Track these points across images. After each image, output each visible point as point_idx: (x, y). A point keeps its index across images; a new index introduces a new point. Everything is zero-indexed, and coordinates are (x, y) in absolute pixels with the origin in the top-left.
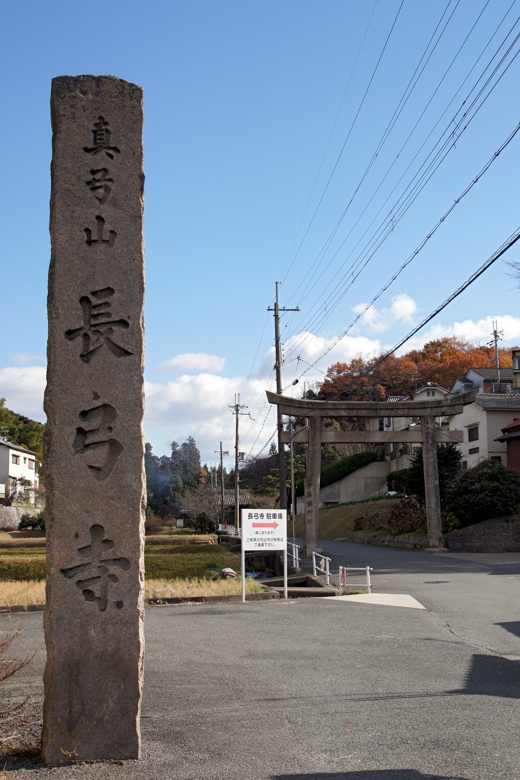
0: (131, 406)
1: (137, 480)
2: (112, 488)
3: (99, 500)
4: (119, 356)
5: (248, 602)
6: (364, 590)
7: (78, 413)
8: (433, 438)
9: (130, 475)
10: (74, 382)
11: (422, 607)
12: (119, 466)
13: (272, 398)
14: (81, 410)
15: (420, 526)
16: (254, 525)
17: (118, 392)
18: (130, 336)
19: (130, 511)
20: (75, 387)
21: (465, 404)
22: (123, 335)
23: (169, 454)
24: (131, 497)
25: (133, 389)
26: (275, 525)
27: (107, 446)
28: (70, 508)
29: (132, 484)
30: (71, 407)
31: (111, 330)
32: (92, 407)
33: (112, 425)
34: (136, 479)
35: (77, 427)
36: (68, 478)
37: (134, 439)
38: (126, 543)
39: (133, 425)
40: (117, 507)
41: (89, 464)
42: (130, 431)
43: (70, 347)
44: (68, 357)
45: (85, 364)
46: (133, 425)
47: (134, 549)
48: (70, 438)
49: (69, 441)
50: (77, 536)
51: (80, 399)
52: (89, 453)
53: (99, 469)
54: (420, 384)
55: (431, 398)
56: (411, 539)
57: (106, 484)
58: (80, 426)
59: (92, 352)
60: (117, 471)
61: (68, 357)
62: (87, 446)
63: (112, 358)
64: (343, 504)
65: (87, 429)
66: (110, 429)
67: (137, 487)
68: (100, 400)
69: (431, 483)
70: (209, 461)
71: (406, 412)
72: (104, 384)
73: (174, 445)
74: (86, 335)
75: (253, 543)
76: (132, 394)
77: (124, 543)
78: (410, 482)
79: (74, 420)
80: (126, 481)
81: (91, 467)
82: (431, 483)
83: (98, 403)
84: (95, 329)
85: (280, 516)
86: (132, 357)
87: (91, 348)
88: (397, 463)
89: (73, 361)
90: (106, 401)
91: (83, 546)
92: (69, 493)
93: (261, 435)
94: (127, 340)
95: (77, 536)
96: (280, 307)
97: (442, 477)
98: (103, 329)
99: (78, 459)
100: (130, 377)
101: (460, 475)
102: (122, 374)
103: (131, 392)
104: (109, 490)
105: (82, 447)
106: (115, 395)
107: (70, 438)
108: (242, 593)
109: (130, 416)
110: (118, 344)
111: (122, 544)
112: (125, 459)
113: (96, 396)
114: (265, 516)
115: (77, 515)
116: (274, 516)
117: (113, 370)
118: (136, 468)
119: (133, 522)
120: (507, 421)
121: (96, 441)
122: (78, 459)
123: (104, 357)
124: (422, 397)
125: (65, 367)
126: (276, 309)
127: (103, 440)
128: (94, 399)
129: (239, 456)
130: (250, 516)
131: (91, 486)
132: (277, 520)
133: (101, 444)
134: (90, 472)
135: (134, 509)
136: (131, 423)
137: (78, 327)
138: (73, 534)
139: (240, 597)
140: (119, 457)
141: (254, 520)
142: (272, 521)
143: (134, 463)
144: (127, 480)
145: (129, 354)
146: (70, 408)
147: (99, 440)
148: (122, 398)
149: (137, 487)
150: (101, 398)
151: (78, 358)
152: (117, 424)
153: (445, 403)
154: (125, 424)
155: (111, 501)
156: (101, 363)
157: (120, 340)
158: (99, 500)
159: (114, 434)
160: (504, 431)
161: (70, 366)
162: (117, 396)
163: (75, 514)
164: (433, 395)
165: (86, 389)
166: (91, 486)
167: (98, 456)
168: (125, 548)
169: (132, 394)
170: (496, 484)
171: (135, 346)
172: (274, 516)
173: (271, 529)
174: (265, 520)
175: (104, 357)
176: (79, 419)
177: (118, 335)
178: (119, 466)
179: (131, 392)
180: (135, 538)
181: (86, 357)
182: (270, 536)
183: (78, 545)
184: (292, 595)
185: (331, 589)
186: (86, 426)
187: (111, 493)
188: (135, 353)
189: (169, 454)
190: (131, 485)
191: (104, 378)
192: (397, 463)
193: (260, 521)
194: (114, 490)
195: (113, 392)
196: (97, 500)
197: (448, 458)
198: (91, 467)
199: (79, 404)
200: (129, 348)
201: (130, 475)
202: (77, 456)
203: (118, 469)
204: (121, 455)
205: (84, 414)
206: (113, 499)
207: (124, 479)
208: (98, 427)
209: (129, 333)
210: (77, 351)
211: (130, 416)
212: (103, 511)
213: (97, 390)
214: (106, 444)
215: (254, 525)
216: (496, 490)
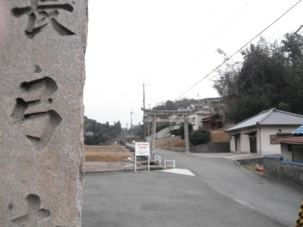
0: (71, 80)
1: (75, 150)
2: (50, 158)
3: (35, 170)
4: (62, 34)
5: (137, 172)
6: (172, 168)
7: (18, 85)
8: (187, 121)
9: (67, 145)
10: (17, 56)
11: (192, 174)
12: (57, 136)
13: (142, 109)
14: (22, 81)
15: (182, 145)
16: (140, 147)
17: (59, 67)
18: (74, 18)
19: (66, 180)
20: (17, 60)
21: (196, 111)
22: (67, 17)
23: (113, 124)
24: (68, 166)
25: (73, 65)
26: (146, 148)
27: (47, 117)
28: (5, 178)
29: (70, 154)
30: (12, 78)
31: (57, 13)
32: (33, 79)
33: (52, 97)
34: (73, 149)
35: (17, 97)
36: (4, 148)
37: (73, 110)
38: (62, 212)
39: (72, 98)
40: (54, 177)
41: (27, 134)
42: (69, 103)
43: (15, 23)
44: (12, 32)
45: (29, 39)
46: (72, 98)
47: (70, 217)
48: (9, 108)
49: (7, 111)
50: (11, 207)
51: (22, 71)
52: (28, 122)
53: (37, 139)
54: (178, 107)
55: (182, 111)
56: (179, 148)
57: (43, 154)
58: (20, 97)
59: (37, 30)
60: (54, 141)
61: (12, 32)
62: (27, 116)
63: (56, 35)
64: (159, 139)
65: (26, 100)
66: (50, 100)
67: (74, 157)
68: (41, 73)
69: (186, 133)
70: (123, 126)
71: (174, 114)
72: (47, 59)
73: (115, 122)
74: (33, 15)
75: (139, 153)
76: (72, 69)
77: (60, 212)
78: (180, 133)
79: (14, 91)
80: (63, 151)
81: (30, 137)
82: (186, 133)
83: (39, 76)
84: (42, 10)
85: (147, 145)
86: (74, 36)
87: (37, 25)
88: (173, 128)
89: (18, 35)
90: (47, 74)
91: (16, 217)
92: (4, 163)
93: (138, 119)
94: (71, 21)
95: (11, 207)
96: (145, 84)
97: (189, 132)
98: (48, 11)
99: (16, 128)
100: (72, 53)
101: (193, 132)
102: (64, 51)
103: (72, 67)
104: (46, 160)
105: (23, 117)
106: (56, 69)
107: (9, 108)
108: (135, 168)
109: (70, 89)
110: (62, 24)
111: (58, 213)
112: (64, 130)
113: (38, 69)
114: (143, 145)
115: (12, 185)
116: (146, 145)
117: (55, 47)
118: (73, 138)
119: (69, 191)
120: (203, 117)
121: (35, 112)
122: (16, 128)
123: (49, 33)
124: (179, 110)
125: (9, 41)
126: (144, 85)
127: (43, 111)
128: (36, 72)
129: (132, 125)
130: (138, 145)
131: (28, 156)
132: (146, 146)
133: (42, 115)
134: (29, 141)
135: (71, 178)
136: (70, 96)
137: (24, 6)
138: (7, 205)
139: (134, 170)
140: (57, 128)
141: (139, 146)
142: (145, 146)
143: (72, 133)
144: (64, 150)
145: (70, 33)
146: (11, 79)
147: (39, 111)
148: (63, 72)
149: (74, 157)
150: (43, 71)
151: (23, 34)
152: (56, 96)
153: (190, 111)
154: (65, 97)
155: (48, 171)
156: (45, 40)
157: (64, 21)
158: (35, 170)
159: (54, 106)
160: (202, 119)
161: (14, 41)
162: (58, 71)
163: (10, 184)
164: (182, 110)
165: (28, 62)
166: (28, 156)
167: (37, 126)
168: (61, 217)
169: (72, 69)
170: (204, 134)
171: (78, 27)
172: (146, 145)
173: (144, 149)
174: (143, 146)
175: (49, 33)
176: (19, 90)
177: (63, 17)
178: (57, 136)
179: (72, 67)
180: (71, 207)
181: (32, 33)
182: (144, 151)
183: (12, 216)
184: (152, 169)
185: (161, 166)
186: (26, 96)
187: (48, 163)
188: (78, 33)
189: (113, 124)
190: (68, 155)
191: (47, 53)
192: (173, 128)
193: (141, 146)
194: (51, 160)
195: (55, 66)
196: (34, 170)
197: (190, 127)
198: (30, 137)
199: (21, 76)
200: (72, 29)
201: (67, 145)
202: (15, 126)
203: (56, 139)
204: (60, 126)
205: (27, 86)
206: (49, 168)
207: (62, 149)
208: (37, 98)
209: (73, 16)
210: (22, 27)
211: (70, 89)
212: (40, 180)
213: (40, 64)
214: (46, 115)
215: (140, 147)
216: (204, 136)
